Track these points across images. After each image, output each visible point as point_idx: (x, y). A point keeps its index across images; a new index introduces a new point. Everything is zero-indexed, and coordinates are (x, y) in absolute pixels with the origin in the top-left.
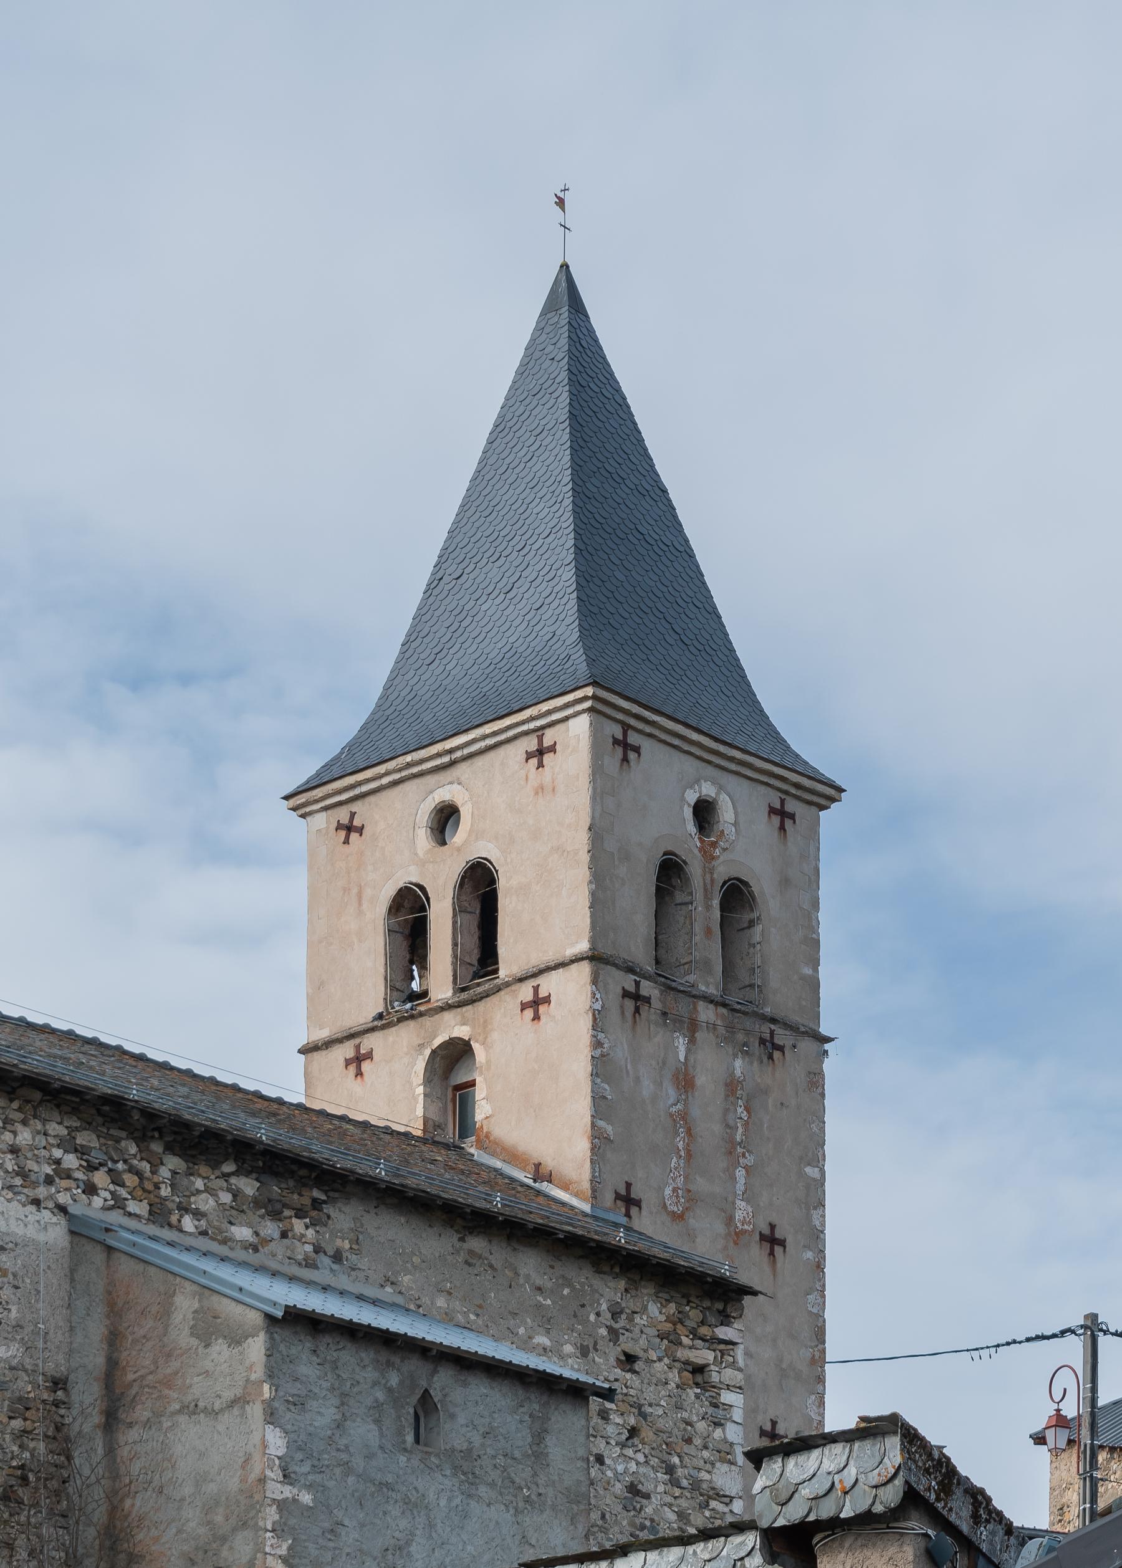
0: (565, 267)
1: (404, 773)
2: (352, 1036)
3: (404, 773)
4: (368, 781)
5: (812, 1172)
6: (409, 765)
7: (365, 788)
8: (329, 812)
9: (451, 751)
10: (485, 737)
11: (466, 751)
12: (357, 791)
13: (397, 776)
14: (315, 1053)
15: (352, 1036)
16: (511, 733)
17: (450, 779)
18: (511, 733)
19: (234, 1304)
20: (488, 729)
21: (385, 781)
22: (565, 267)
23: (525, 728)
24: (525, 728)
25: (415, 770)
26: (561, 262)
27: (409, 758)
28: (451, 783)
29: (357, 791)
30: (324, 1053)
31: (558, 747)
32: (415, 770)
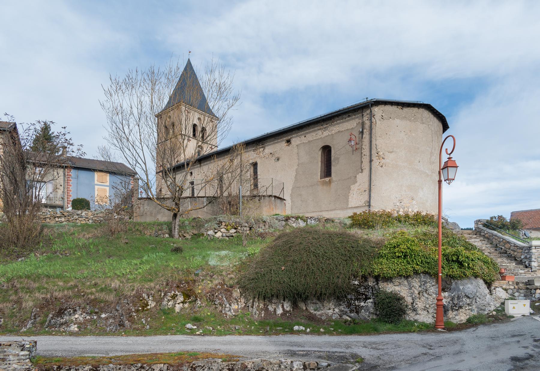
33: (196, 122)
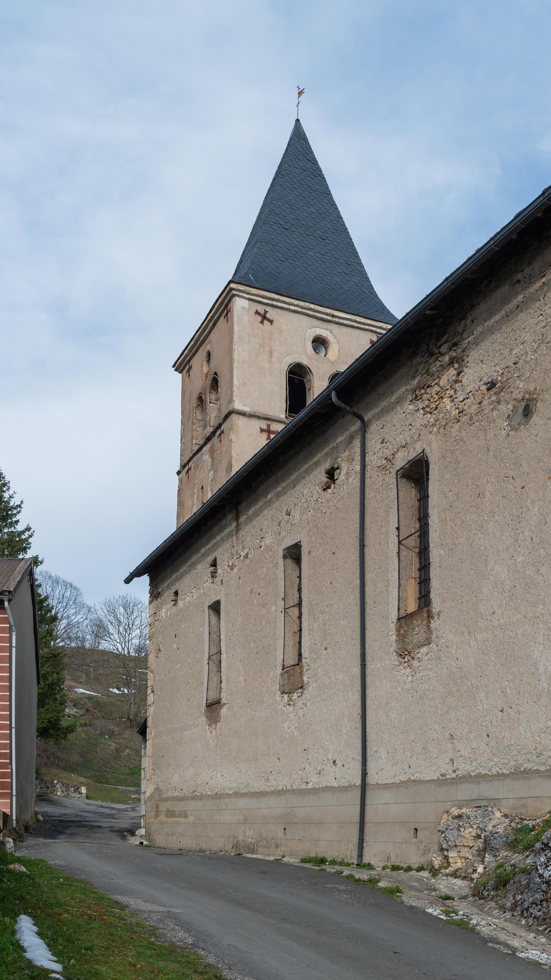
0: (298, 121)
1: (304, 311)
2: (267, 419)
3: (304, 311)
4: (284, 302)
5: (74, 650)
6: (310, 309)
7: (279, 304)
8: (251, 302)
9: (333, 316)
10: (355, 321)
11: (341, 321)
12: (275, 303)
13: (300, 310)
14: (241, 416)
15: (267, 419)
16: (366, 327)
17: (325, 327)
18: (366, 327)
19: (406, 540)
20: (358, 319)
21: (292, 308)
22: (298, 121)
23: (374, 329)
24: (374, 329)
25: (311, 313)
26: (296, 118)
27: (313, 306)
28: (327, 330)
29: (275, 303)
30: (246, 419)
31: (261, 324)
32: (311, 313)
33: (305, 356)
